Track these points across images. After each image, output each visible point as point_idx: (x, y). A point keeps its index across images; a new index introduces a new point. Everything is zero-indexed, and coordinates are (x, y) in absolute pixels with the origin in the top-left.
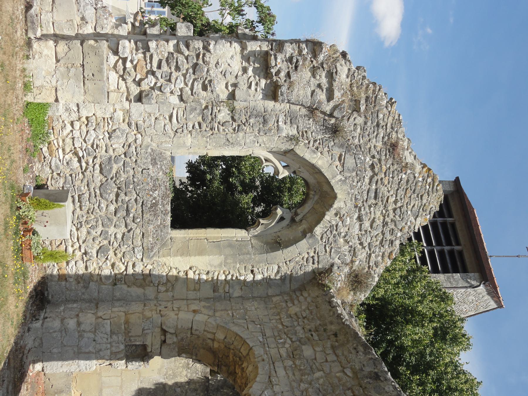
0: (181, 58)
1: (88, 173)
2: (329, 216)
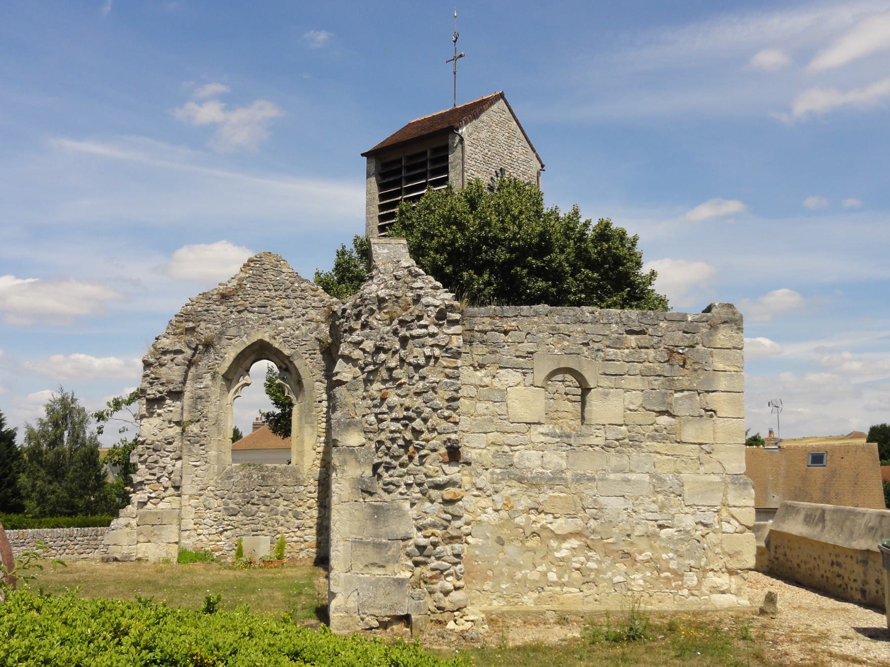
0: (149, 460)
1: (236, 525)
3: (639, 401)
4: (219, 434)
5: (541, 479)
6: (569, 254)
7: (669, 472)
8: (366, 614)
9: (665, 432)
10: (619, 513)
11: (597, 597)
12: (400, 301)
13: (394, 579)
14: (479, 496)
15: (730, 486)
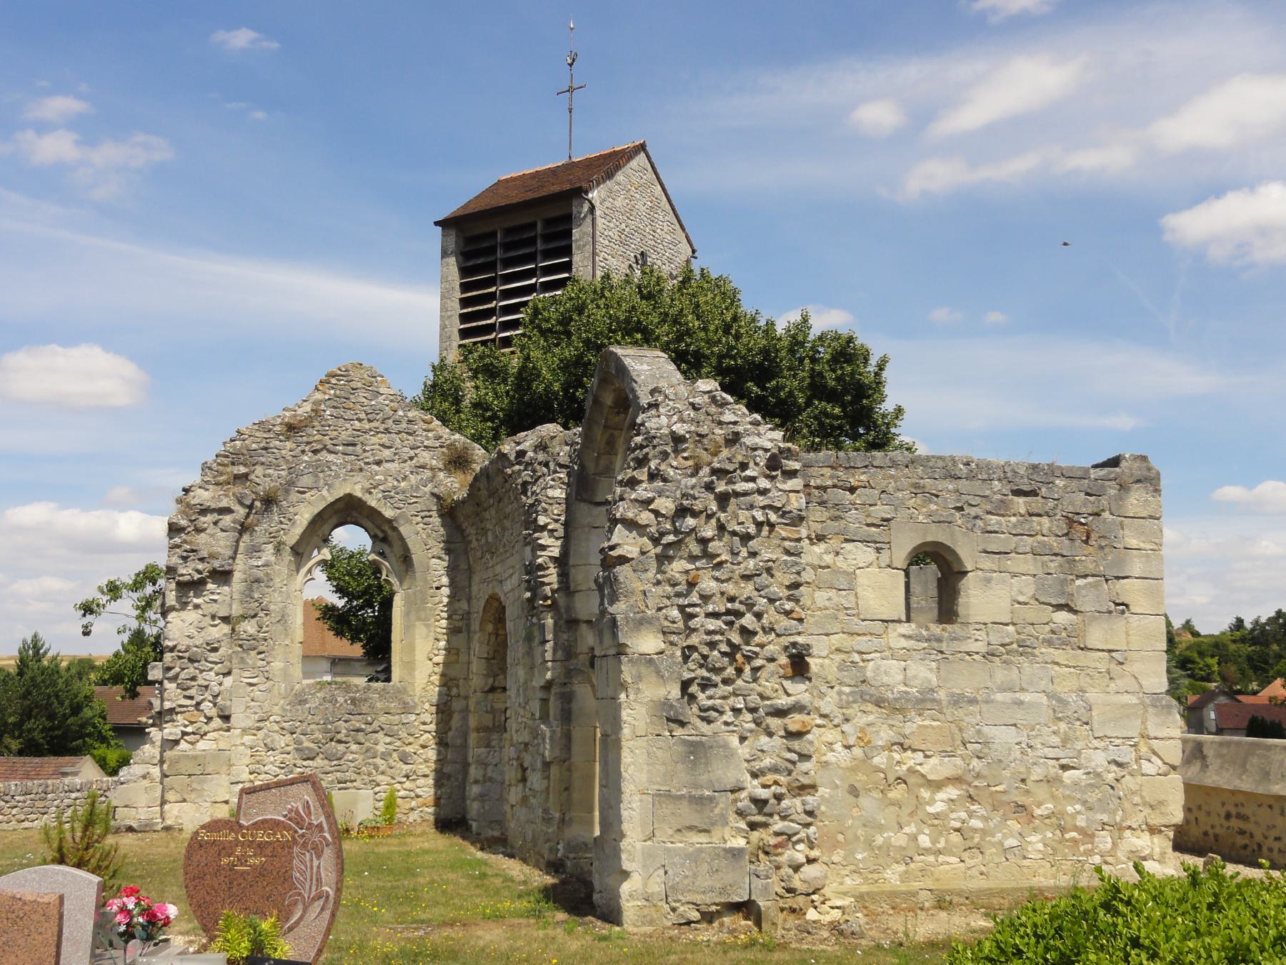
0: (182, 676)
3: (1030, 590)
4: (287, 635)
5: (908, 700)
6: (803, 379)
7: (1071, 691)
8: (679, 901)
9: (1064, 634)
10: (1010, 749)
11: (983, 869)
12: (705, 441)
13: (725, 850)
14: (824, 726)
15: (1150, 710)
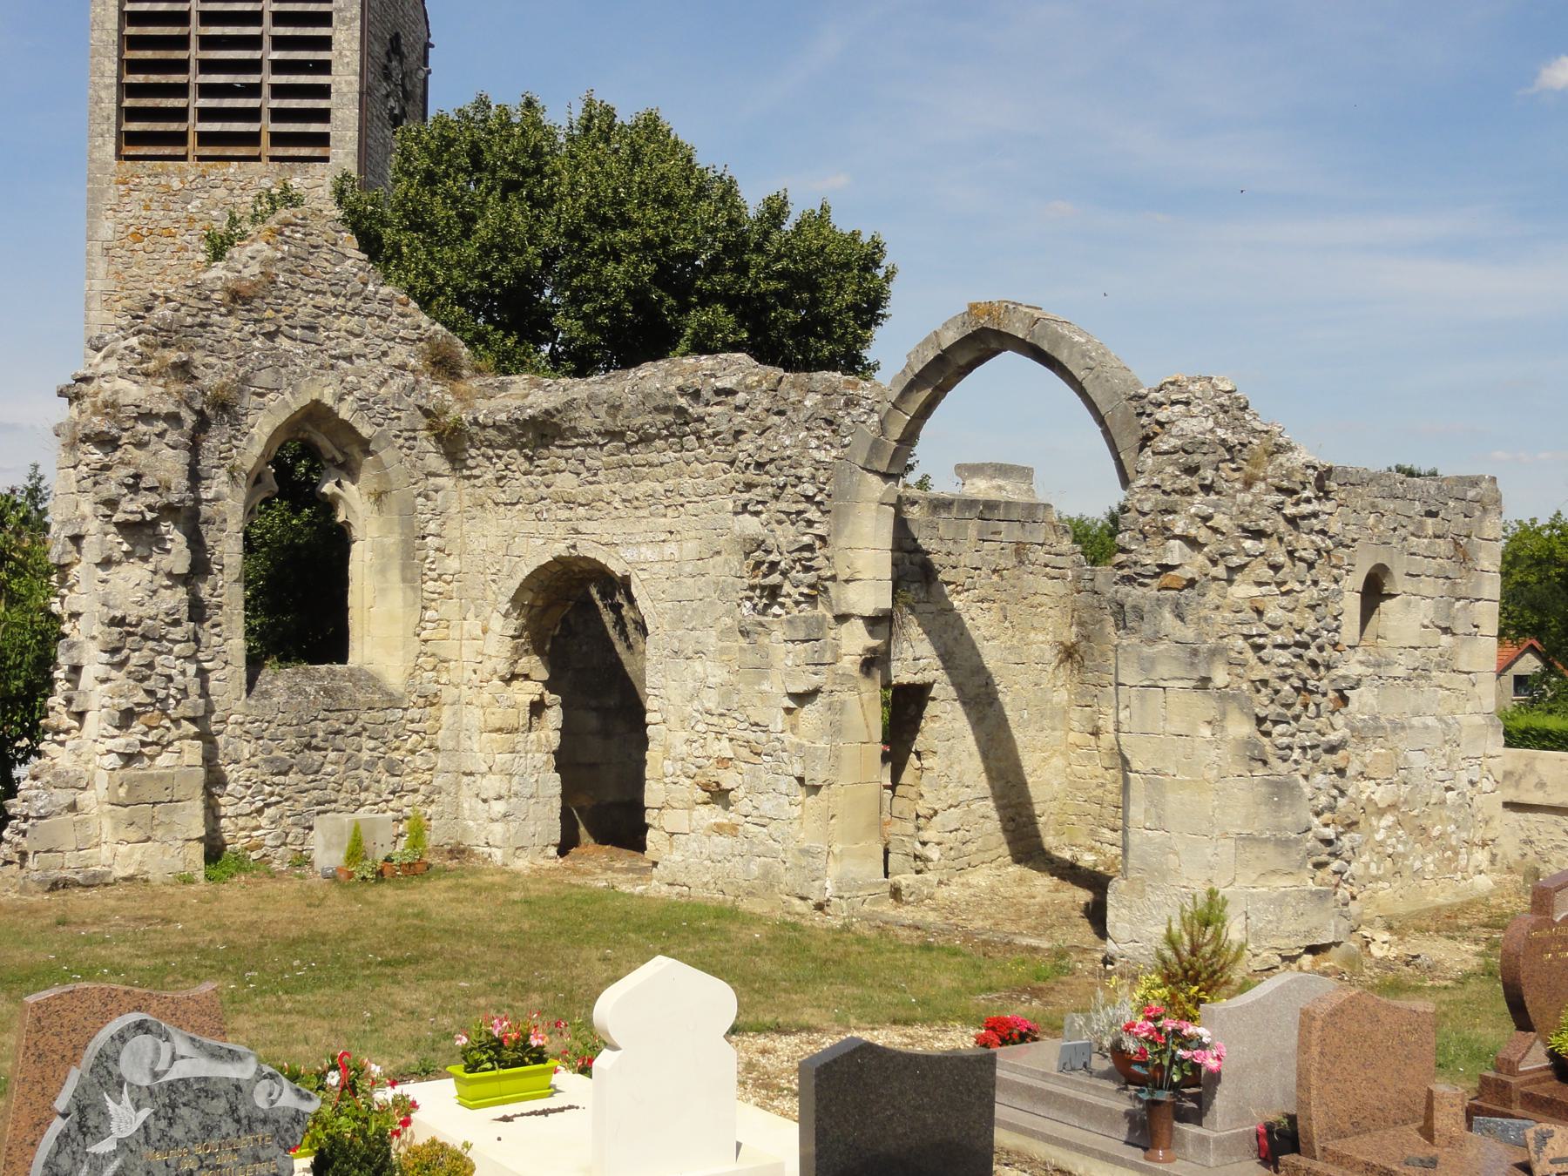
2: (344, 412)
